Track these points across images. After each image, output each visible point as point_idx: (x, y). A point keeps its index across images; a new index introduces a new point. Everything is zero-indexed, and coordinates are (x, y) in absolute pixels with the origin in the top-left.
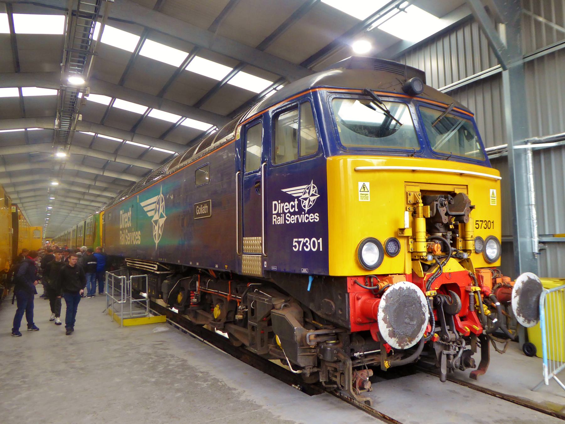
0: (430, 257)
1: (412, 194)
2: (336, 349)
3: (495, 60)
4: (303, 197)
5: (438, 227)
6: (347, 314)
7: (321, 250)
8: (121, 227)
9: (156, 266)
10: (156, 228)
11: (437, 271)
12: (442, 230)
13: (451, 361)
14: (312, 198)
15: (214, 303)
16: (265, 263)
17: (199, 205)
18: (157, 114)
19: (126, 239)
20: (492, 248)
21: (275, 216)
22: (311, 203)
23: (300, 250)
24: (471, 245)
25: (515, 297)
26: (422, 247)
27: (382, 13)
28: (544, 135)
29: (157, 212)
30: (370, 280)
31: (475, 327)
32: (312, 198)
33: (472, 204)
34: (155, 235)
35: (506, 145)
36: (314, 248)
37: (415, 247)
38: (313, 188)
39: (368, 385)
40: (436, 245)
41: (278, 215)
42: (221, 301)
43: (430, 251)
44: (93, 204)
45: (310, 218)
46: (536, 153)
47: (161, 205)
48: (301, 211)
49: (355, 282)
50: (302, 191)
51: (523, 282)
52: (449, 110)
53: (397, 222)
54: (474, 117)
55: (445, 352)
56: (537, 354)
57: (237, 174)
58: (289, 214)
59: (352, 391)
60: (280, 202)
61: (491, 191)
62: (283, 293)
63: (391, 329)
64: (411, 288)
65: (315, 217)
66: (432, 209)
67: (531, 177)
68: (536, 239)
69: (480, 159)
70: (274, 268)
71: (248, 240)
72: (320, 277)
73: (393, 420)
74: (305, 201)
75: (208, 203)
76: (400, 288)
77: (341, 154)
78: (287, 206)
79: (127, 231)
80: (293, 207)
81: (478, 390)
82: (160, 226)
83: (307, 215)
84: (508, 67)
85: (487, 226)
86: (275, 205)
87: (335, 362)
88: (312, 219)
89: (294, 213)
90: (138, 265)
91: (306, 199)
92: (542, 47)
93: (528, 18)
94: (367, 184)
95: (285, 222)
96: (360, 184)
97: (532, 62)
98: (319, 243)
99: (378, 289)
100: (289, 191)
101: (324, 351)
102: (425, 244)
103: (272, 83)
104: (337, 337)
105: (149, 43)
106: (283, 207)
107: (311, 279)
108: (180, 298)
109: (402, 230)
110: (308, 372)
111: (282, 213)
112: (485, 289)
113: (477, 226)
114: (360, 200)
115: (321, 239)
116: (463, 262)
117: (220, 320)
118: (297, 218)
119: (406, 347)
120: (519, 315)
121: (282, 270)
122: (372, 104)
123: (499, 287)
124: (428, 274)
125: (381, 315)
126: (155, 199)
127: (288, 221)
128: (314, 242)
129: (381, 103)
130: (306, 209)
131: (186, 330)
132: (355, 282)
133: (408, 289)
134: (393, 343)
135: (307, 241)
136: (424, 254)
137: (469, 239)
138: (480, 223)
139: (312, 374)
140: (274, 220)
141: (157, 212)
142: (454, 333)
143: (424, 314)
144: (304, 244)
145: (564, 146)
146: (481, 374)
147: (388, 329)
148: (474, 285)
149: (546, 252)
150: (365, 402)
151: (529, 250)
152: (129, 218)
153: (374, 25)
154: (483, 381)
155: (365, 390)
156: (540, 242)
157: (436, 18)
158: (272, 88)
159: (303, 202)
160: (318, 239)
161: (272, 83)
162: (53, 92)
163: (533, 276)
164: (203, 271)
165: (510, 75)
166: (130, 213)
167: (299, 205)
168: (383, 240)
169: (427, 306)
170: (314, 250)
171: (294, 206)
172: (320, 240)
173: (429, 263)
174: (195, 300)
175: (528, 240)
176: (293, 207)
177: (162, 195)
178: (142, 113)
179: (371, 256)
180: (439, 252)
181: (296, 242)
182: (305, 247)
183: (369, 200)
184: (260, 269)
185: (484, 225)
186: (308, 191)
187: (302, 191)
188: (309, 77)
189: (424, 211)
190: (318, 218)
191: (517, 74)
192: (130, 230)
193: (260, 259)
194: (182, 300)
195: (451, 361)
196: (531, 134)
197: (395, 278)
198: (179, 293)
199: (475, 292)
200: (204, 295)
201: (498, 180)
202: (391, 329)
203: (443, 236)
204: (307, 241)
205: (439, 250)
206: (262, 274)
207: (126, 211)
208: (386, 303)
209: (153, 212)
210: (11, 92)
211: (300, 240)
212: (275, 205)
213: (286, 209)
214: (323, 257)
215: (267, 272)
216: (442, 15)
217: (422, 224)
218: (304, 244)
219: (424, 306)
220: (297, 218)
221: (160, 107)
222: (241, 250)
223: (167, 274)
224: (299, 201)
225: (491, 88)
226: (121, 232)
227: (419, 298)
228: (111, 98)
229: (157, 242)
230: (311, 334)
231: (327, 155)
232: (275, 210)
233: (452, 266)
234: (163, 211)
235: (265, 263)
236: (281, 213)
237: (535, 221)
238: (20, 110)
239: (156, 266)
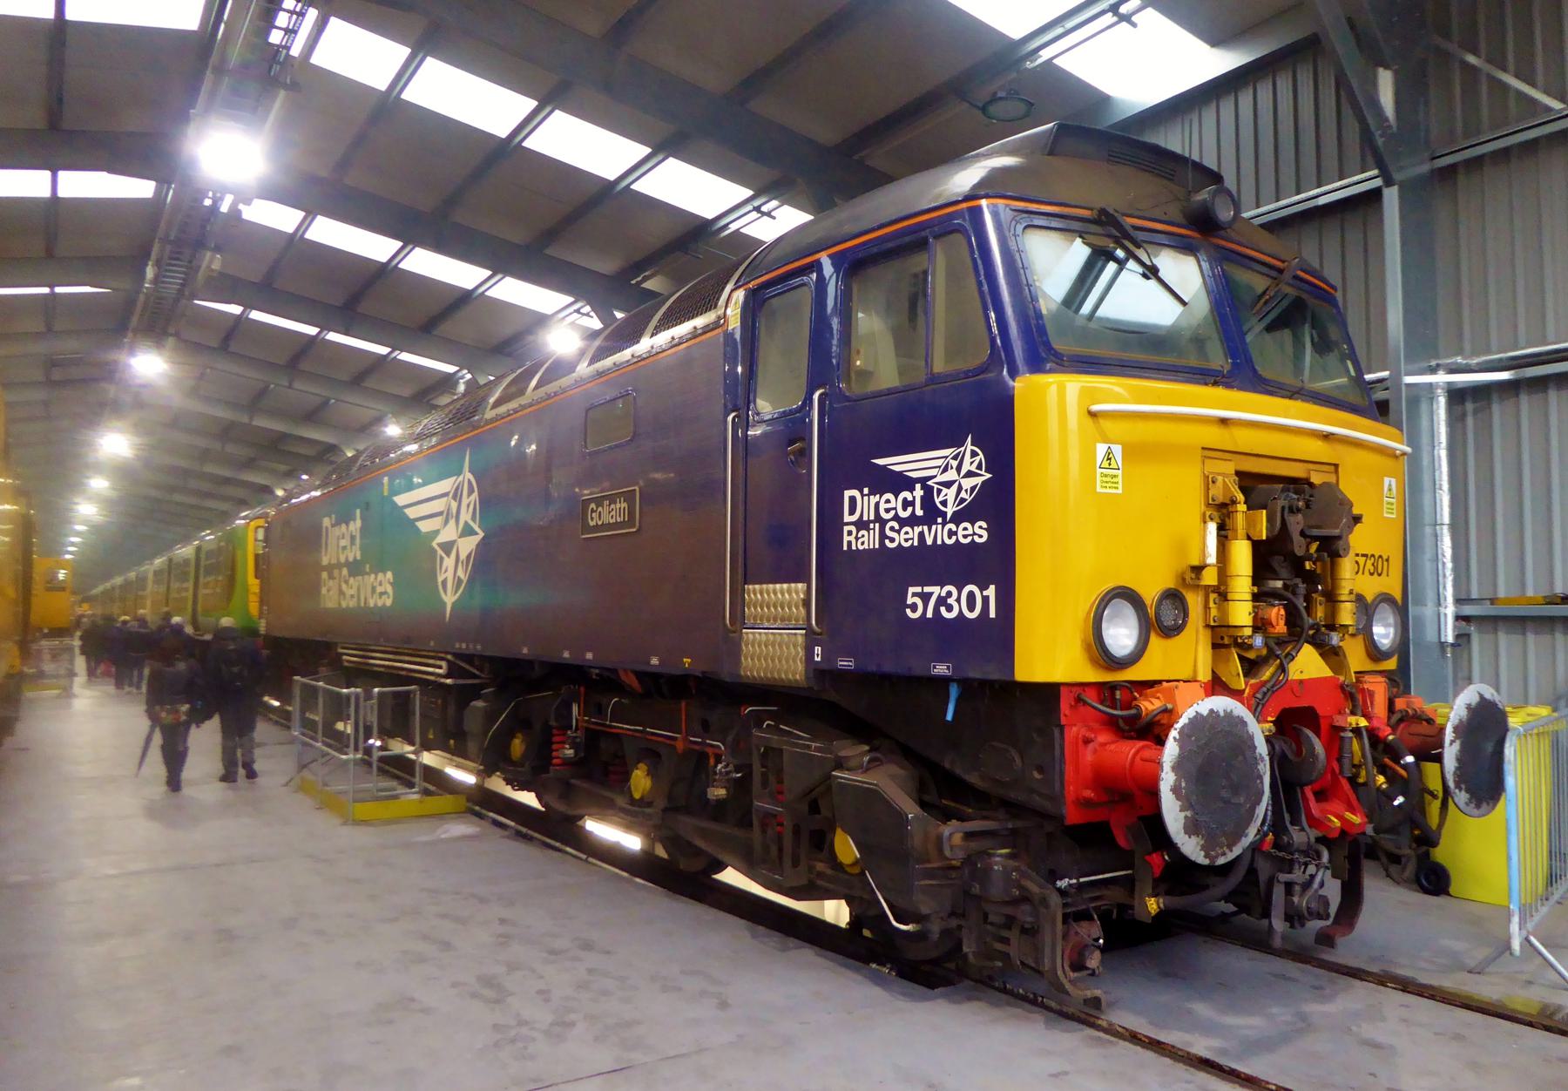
0: (1258, 641)
1: (1220, 479)
2: (1016, 869)
3: (1370, 159)
4: (940, 478)
5: (1276, 565)
6: (1057, 777)
7: (992, 615)
8: (325, 561)
9: (444, 664)
10: (449, 562)
11: (1273, 675)
12: (1284, 573)
13: (1296, 899)
14: (968, 483)
16: (818, 650)
17: (598, 502)
18: (426, 263)
19: (341, 593)
20: (1386, 626)
21: (853, 528)
22: (963, 495)
23: (929, 615)
24: (1347, 615)
25: (1452, 742)
26: (1241, 613)
27: (1070, 24)
28: (1475, 353)
29: (452, 522)
30: (1113, 694)
31: (1349, 815)
32: (968, 483)
33: (1355, 511)
34: (444, 583)
35: (1385, 374)
37: (1224, 612)
38: (971, 456)
39: (1094, 961)
40: (1275, 610)
41: (861, 525)
42: (651, 755)
43: (1260, 625)
44: (210, 504)
45: (961, 533)
46: (1457, 396)
47: (465, 501)
48: (932, 513)
49: (1079, 700)
50: (939, 462)
51: (1469, 707)
52: (1287, 276)
53: (1181, 547)
54: (1339, 295)
55: (1283, 877)
56: (1452, 890)
57: (730, 418)
59: (1060, 972)
60: (866, 491)
61: (1387, 480)
62: (858, 729)
63: (1189, 814)
64: (1236, 713)
65: (978, 532)
66: (1270, 520)
67: (1443, 454)
68: (1450, 610)
69: (1354, 398)
70: (845, 663)
71: (756, 592)
72: (985, 684)
73: (1159, 1043)
74: (945, 490)
75: (629, 497)
76: (1212, 711)
77: (1050, 371)
78: (890, 503)
79: (345, 571)
80: (907, 504)
81: (1337, 971)
82: (463, 556)
84: (1397, 176)
85: (1376, 568)
86: (853, 500)
87: (1015, 902)
88: (965, 537)
89: (913, 521)
90: (379, 662)
91: (948, 484)
92: (1479, 132)
93: (1445, 56)
94: (1117, 450)
95: (882, 543)
96: (1101, 449)
97: (1453, 168)
98: (986, 600)
99: (1138, 716)
100: (897, 463)
101: (984, 875)
102: (1248, 607)
103: (750, 193)
104: (1011, 838)
105: (433, 68)
106: (877, 505)
107: (954, 691)
108: (518, 746)
109: (1198, 570)
110: (935, 928)
111: (871, 520)
112: (1376, 723)
114: (1099, 489)
115: (992, 587)
116: (1331, 654)
117: (649, 804)
118: (921, 535)
119: (1221, 861)
120: (1458, 786)
121: (872, 668)
123: (1401, 720)
124: (1252, 681)
125: (1167, 780)
126: (446, 485)
127: (892, 540)
128: (971, 595)
129: (1139, 247)
131: (531, 833)
132: (1079, 700)
133: (1229, 715)
134: (1191, 848)
135: (949, 594)
136: (1248, 632)
137: (1343, 598)
139: (946, 933)
140: (846, 538)
141: (452, 522)
142: (1303, 830)
143: (1261, 777)
145: (1535, 382)
146: (1344, 935)
147: (1183, 814)
148: (1353, 713)
149: (1469, 641)
150: (1086, 1001)
151: (1430, 636)
152: (353, 538)
153: (1045, 54)
154: (1346, 951)
155: (1085, 973)
156: (1458, 618)
157: (1203, 47)
158: (749, 207)
159: (939, 491)
160: (983, 588)
161: (750, 193)
162: (140, 188)
163: (1489, 693)
164: (606, 674)
165: (1401, 197)
166: (356, 526)
167: (928, 500)
168: (1150, 593)
169: (1267, 758)
171: (912, 504)
172: (991, 591)
173: (1251, 655)
174: (570, 752)
175: (1428, 611)
176: (907, 504)
177: (469, 476)
178: (383, 258)
179: (1121, 635)
180: (1281, 628)
181: (914, 595)
182: (943, 609)
183: (1120, 491)
184: (800, 667)
185: (1369, 566)
186: (955, 463)
187: (939, 462)
188: (938, 172)
189: (1250, 523)
190: (985, 534)
191: (1417, 196)
192: (355, 569)
193: (800, 640)
194: (524, 755)
195: (1296, 899)
196: (1467, 346)
197: (1182, 692)
198: (513, 737)
199: (1357, 731)
200: (592, 740)
201: (1404, 454)
202: (1189, 814)
203: (1286, 586)
204: (949, 594)
205: (1282, 622)
206: (807, 678)
207: (345, 519)
208: (1181, 748)
209: (439, 520)
210: (29, 184)
211: (927, 589)
212: (853, 500)
213: (887, 511)
214: (998, 634)
215: (821, 674)
216: (1217, 38)
217: (1242, 554)
218: (942, 601)
219: (1262, 759)
220: (921, 535)
221: (441, 245)
222: (739, 619)
223: (482, 686)
224: (928, 491)
225: (1343, 230)
226: (325, 575)
227: (1251, 738)
228: (302, 214)
229: (449, 599)
230: (952, 832)
231: (1013, 373)
232: (852, 512)
233: (1307, 664)
234: (473, 519)
235: (818, 650)
236: (869, 521)
237: (1449, 565)
238: (38, 236)
239: (444, 664)
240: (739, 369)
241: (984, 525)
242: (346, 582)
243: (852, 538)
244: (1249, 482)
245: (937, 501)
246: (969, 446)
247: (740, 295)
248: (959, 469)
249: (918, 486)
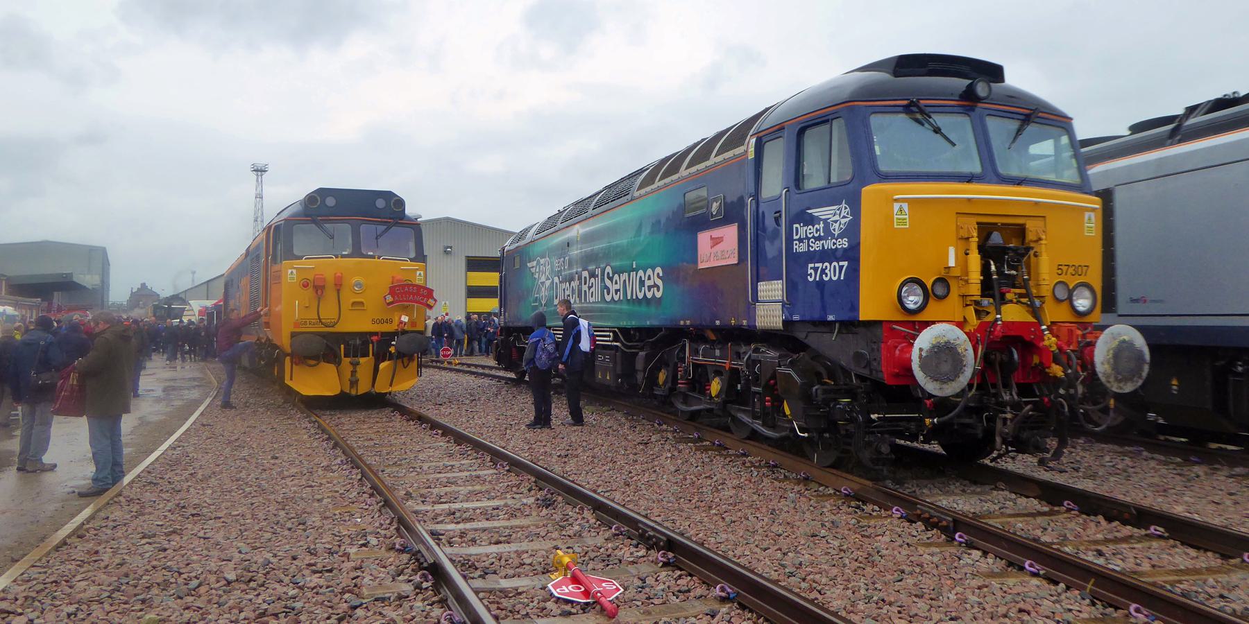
14: (843, 221)
15: (711, 375)
32: (843, 221)
38: (845, 209)
41: (801, 240)
42: (718, 373)
48: (828, 233)
78: (811, 230)
80: (817, 230)
85: (1076, 272)
89: (819, 238)
130: (836, 233)
144: (823, 271)
170: (835, 279)
176: (817, 230)
179: (913, 300)
222: (756, 299)
240: (1016, 356)
242: (611, 279)
244: (985, 230)
247: (754, 140)
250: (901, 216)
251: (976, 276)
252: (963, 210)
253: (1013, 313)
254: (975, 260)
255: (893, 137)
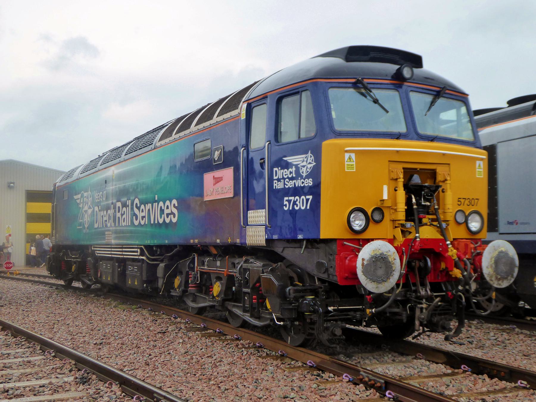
9: (139, 250)
14: (309, 166)
21: (276, 181)
22: (308, 170)
23: (291, 209)
32: (309, 166)
36: (303, 206)
38: (310, 157)
41: (279, 180)
45: (305, 182)
48: (298, 175)
58: (287, 180)
78: (286, 173)
80: (291, 173)
83: (303, 180)
86: (276, 171)
89: (292, 179)
91: (304, 166)
100: (289, 159)
107: (305, 242)
113: (459, 203)
118: (295, 183)
122: (66, 198)
138: (463, 201)
140: (275, 185)
144: (295, 203)
170: (303, 208)
176: (291, 173)
179: (358, 224)
181: (286, 200)
182: (295, 206)
185: (467, 202)
186: (306, 159)
187: (301, 159)
190: (311, 182)
193: (264, 229)
211: (290, 198)
212: (276, 171)
213: (286, 175)
220: (295, 183)
222: (246, 224)
232: (276, 176)
241: (311, 180)
243: (276, 185)
244: (409, 173)
245: (301, 172)
246: (310, 154)
248: (307, 162)
249: (294, 167)
250: (350, 162)
251: (402, 206)
252: (393, 159)
253: (428, 232)
254: (401, 195)
255: (345, 105)
